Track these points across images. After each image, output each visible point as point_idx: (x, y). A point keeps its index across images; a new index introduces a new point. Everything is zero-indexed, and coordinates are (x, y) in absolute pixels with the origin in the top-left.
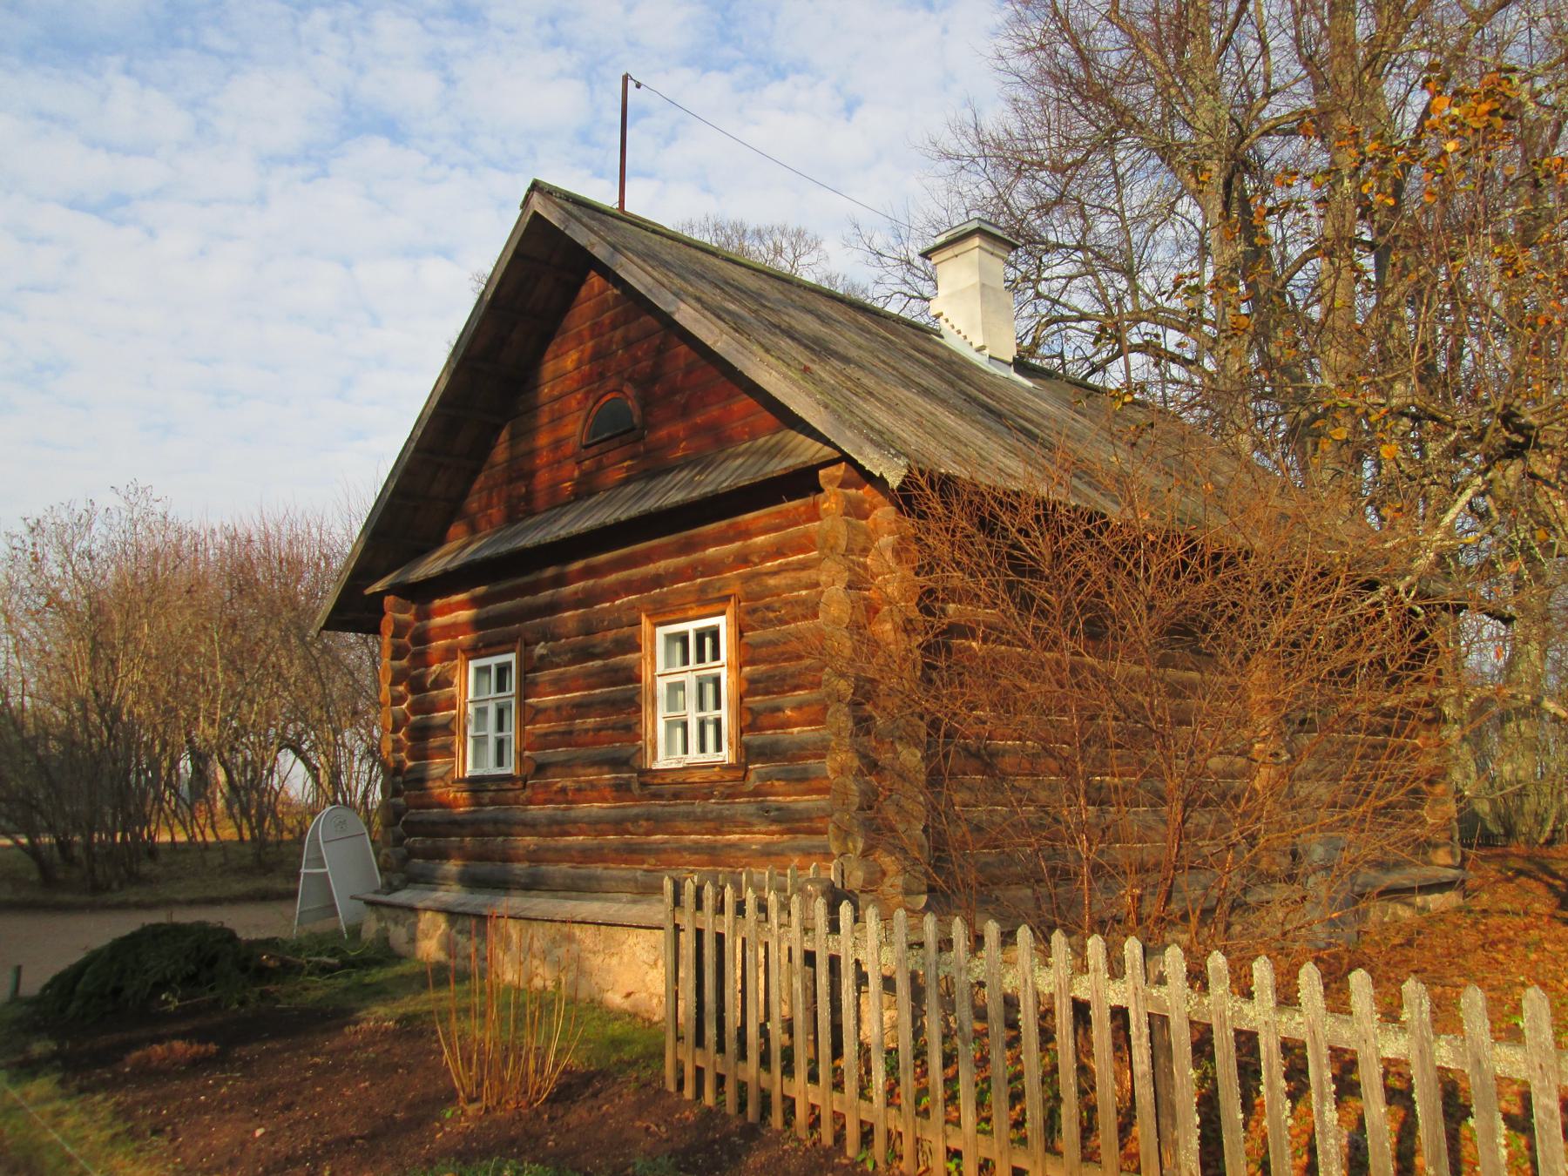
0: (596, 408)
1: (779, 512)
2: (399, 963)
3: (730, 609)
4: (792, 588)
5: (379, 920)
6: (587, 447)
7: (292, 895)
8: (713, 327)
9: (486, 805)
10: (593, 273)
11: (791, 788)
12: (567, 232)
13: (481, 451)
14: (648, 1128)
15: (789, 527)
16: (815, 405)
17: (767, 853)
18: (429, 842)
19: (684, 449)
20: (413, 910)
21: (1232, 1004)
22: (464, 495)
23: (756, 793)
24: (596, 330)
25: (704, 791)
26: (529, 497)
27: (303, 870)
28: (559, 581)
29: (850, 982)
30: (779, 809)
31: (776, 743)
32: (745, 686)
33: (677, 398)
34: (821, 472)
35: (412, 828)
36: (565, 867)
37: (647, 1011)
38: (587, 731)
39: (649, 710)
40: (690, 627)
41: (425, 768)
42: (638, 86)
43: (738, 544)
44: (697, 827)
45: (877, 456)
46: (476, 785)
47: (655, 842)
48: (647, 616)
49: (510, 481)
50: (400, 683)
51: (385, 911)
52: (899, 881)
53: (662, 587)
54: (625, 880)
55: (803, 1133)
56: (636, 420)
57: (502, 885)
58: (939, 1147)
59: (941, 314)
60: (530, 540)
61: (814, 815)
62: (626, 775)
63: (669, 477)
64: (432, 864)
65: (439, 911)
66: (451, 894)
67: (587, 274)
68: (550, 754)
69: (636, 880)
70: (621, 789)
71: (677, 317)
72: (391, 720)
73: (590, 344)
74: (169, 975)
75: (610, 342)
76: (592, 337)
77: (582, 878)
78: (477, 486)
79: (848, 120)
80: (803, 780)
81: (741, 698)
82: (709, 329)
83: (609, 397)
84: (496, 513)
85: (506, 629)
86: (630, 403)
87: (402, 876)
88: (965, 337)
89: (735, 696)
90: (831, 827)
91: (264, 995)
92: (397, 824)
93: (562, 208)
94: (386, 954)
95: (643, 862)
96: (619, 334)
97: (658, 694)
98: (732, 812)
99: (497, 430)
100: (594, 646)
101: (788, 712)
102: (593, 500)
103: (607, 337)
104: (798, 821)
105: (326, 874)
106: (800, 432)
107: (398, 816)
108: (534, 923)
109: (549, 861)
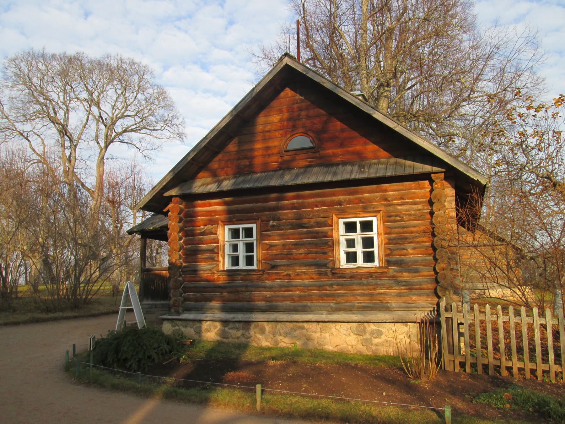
5: (174, 326)
12: (308, 75)
18: (198, 295)
20: (200, 321)
25: (370, 275)
26: (251, 165)
27: (121, 307)
37: (348, 351)
47: (340, 293)
49: (239, 159)
68: (278, 262)
78: (217, 159)
92: (179, 288)
96: (304, 113)
100: (305, 224)
108: (280, 323)
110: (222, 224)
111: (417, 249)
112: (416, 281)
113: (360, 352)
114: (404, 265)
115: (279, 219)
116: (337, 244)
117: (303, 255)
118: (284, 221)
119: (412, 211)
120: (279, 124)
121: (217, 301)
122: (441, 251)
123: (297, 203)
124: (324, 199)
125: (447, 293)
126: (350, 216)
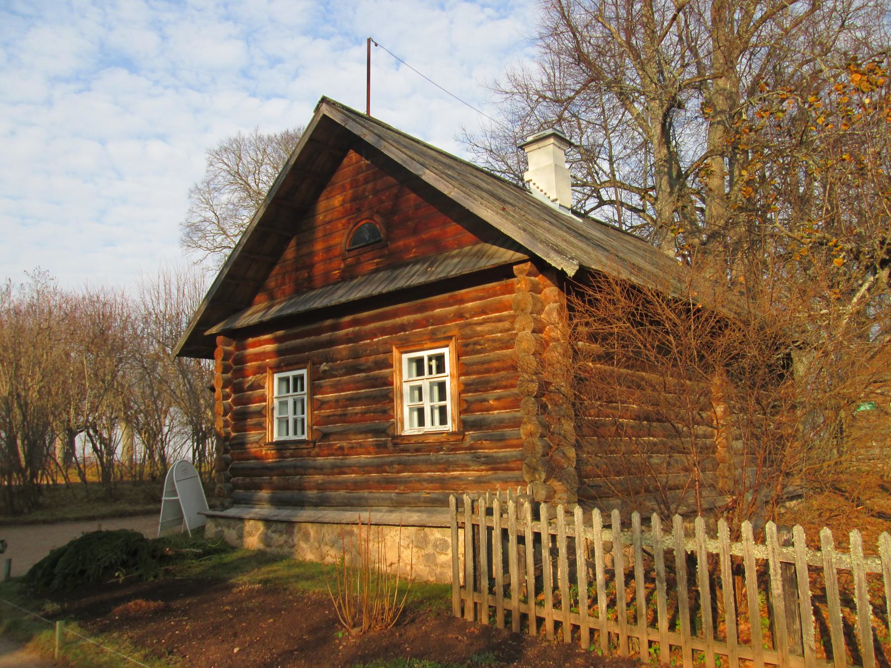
0: (354, 229)
1: (484, 289)
2: (234, 551)
3: (452, 344)
4: (492, 332)
5: (217, 526)
6: (349, 251)
7: (158, 511)
8: (448, 184)
9: (287, 458)
10: (351, 151)
11: (494, 444)
13: (277, 253)
14: (457, 638)
15: (489, 298)
16: (517, 229)
17: (479, 481)
18: (248, 480)
19: (415, 253)
20: (241, 519)
21: (835, 555)
22: (266, 277)
23: (471, 448)
24: (354, 184)
25: (438, 447)
26: (310, 279)
27: (164, 498)
28: (335, 328)
29: (582, 551)
30: (485, 457)
31: (484, 419)
32: (462, 387)
33: (410, 223)
34: (515, 267)
35: (235, 472)
36: (342, 492)
37: (404, 574)
38: (356, 414)
39: (399, 402)
40: (425, 354)
41: (245, 436)
42: (376, 45)
43: (456, 307)
44: (433, 468)
45: (559, 259)
46: (280, 446)
47: (403, 477)
48: (397, 348)
49: (297, 270)
50: (227, 387)
51: (222, 521)
52: (565, 496)
53: (406, 331)
54: (384, 499)
55: (551, 637)
56: (382, 236)
57: (300, 504)
58: (645, 640)
59: (531, 180)
60: (319, 304)
61: (509, 460)
62: (384, 439)
63: (408, 269)
64: (249, 493)
65: (259, 520)
66: (266, 510)
67: (348, 151)
68: (331, 428)
69: (392, 499)
70: (380, 447)
71: (423, 178)
72: (222, 409)
73: (350, 192)
74: (113, 561)
75: (364, 191)
76: (352, 188)
77: (354, 498)
78: (274, 272)
79: (397, 70)
80: (501, 440)
81: (460, 394)
82: (445, 185)
83: (364, 222)
84: (288, 287)
85: (300, 355)
86: (378, 226)
87: (230, 500)
88: (545, 194)
89: (456, 394)
90: (524, 466)
91: (167, 572)
92: (226, 470)
93: (342, 113)
94: (226, 547)
95: (396, 489)
96: (370, 186)
97: (404, 392)
98: (456, 459)
99: (288, 240)
100: (361, 365)
101: (491, 402)
102: (355, 281)
103: (361, 188)
104: (499, 463)
105: (178, 500)
106: (493, 244)
107: (227, 464)
108: (326, 525)
109: (331, 489)
110: (271, 372)
111: (503, 400)
112: (501, 455)
113: (420, 576)
114: (485, 428)
115: (333, 360)
116: (399, 395)
117: (359, 415)
118: (339, 362)
119: (497, 332)
120: (340, 209)
121: (266, 489)
122: (527, 401)
123: (353, 332)
124: (386, 322)
125: (537, 476)
126: (415, 348)
